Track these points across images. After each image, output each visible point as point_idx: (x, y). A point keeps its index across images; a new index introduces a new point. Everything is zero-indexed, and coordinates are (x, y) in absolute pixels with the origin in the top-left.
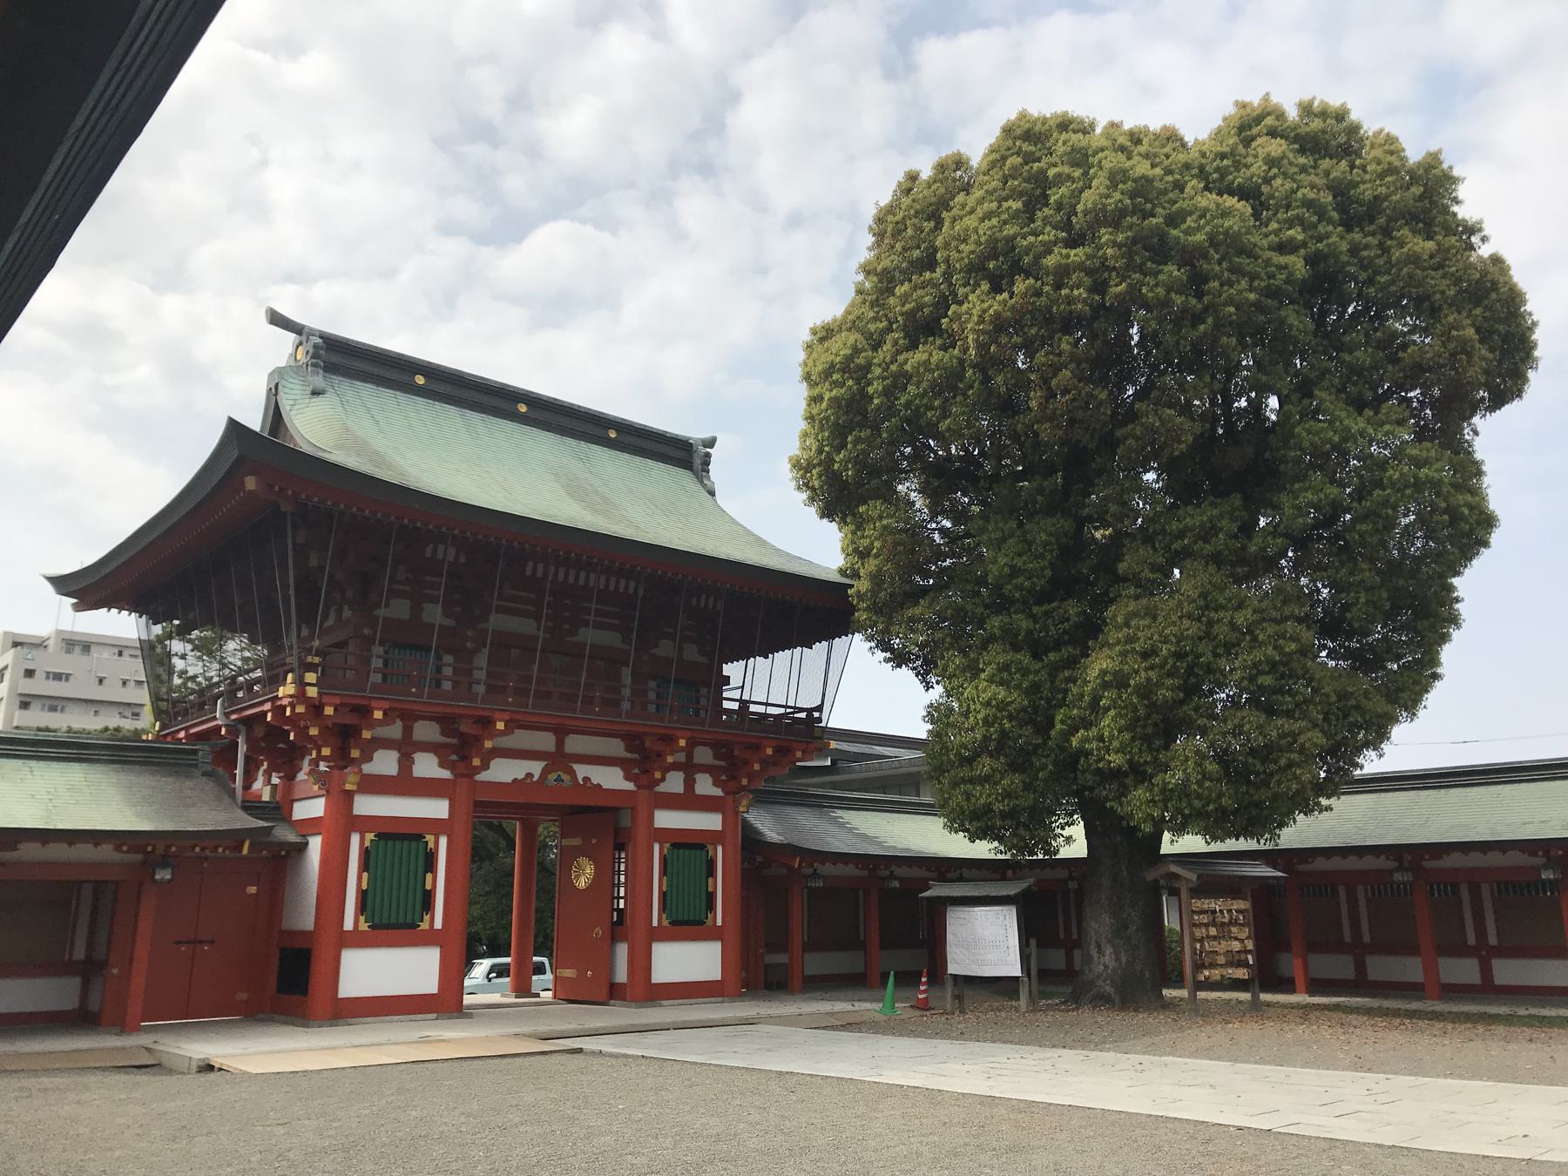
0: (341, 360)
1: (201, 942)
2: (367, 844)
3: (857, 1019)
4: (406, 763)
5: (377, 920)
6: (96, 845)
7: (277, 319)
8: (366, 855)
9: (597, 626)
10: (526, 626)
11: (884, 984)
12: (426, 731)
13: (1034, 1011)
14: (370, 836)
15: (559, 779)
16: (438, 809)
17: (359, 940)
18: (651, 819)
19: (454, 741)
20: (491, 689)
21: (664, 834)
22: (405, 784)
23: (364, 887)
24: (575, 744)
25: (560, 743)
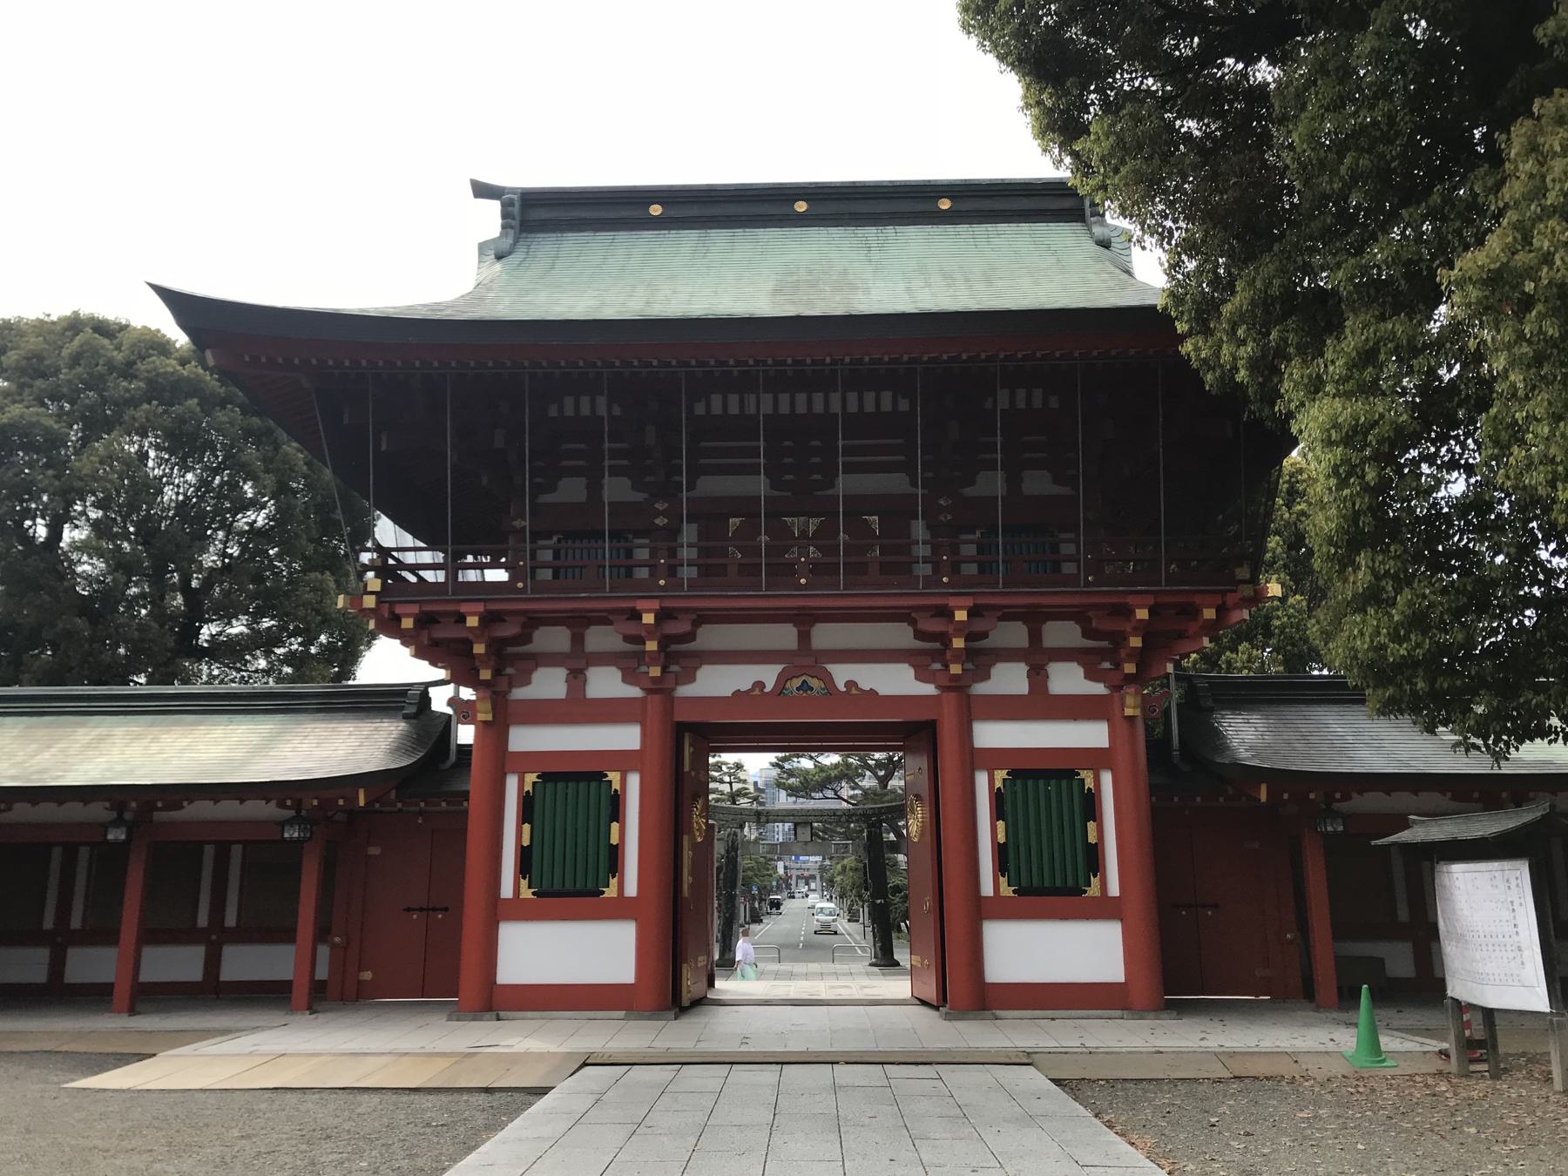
0: (539, 216)
1: (434, 909)
2: (998, 784)
3: (1261, 1068)
4: (1038, 675)
5: (1024, 883)
6: (242, 801)
7: (482, 191)
8: (998, 799)
9: (850, 469)
10: (894, 483)
11: (1356, 1005)
12: (1063, 633)
13: (1467, 1075)
14: (1001, 775)
15: (805, 686)
16: (626, 737)
17: (520, 911)
18: (967, 734)
19: (1105, 644)
20: (705, 571)
21: (528, 760)
22: (1040, 704)
23: (526, 842)
24: (826, 636)
25: (804, 637)
